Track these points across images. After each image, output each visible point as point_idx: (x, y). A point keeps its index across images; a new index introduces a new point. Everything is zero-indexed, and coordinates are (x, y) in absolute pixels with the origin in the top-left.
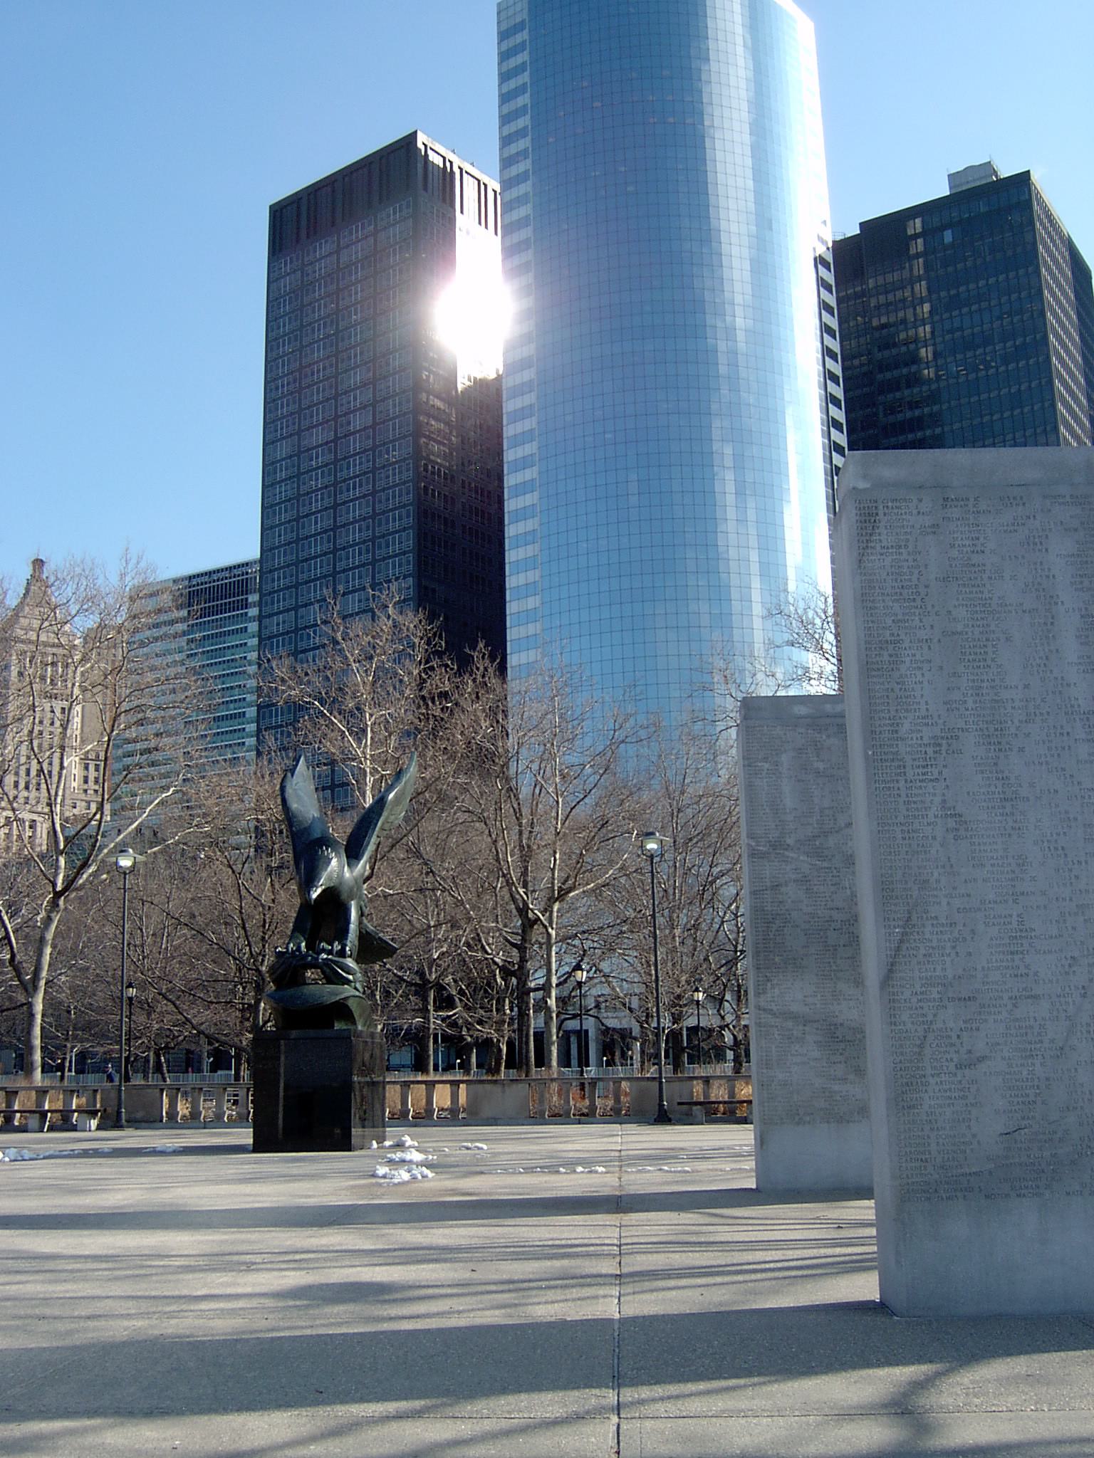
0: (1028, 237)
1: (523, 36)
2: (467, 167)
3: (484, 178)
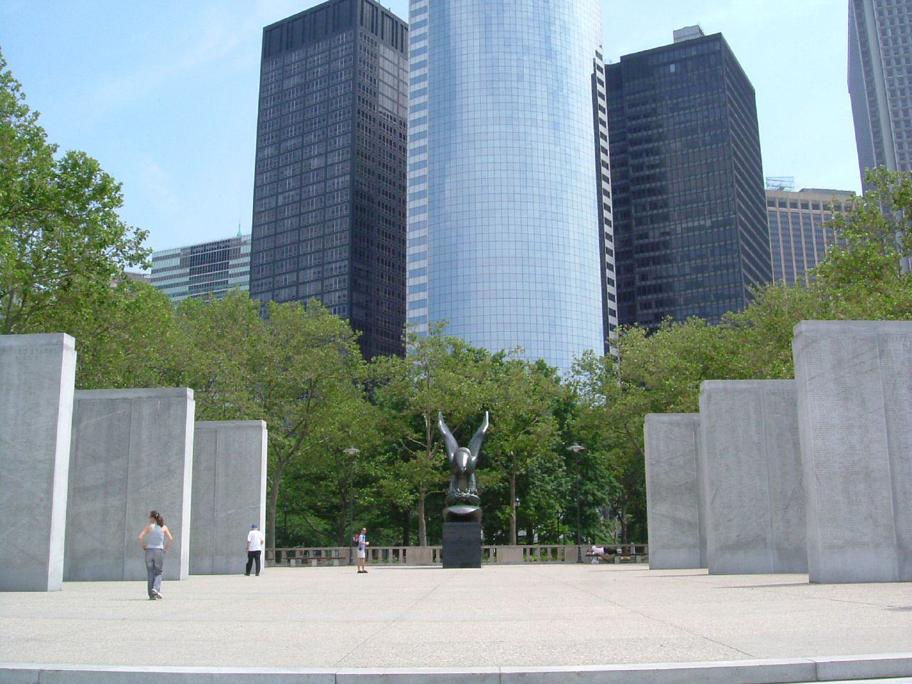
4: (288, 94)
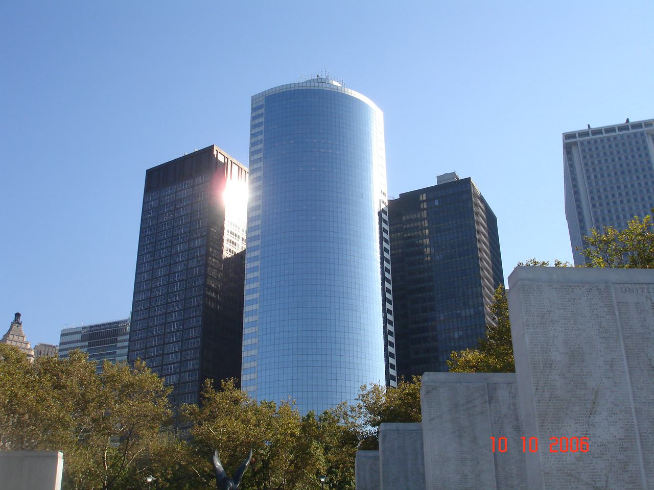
0: (479, 289)
1: (262, 111)
2: (234, 161)
3: (241, 166)
4: (161, 226)
